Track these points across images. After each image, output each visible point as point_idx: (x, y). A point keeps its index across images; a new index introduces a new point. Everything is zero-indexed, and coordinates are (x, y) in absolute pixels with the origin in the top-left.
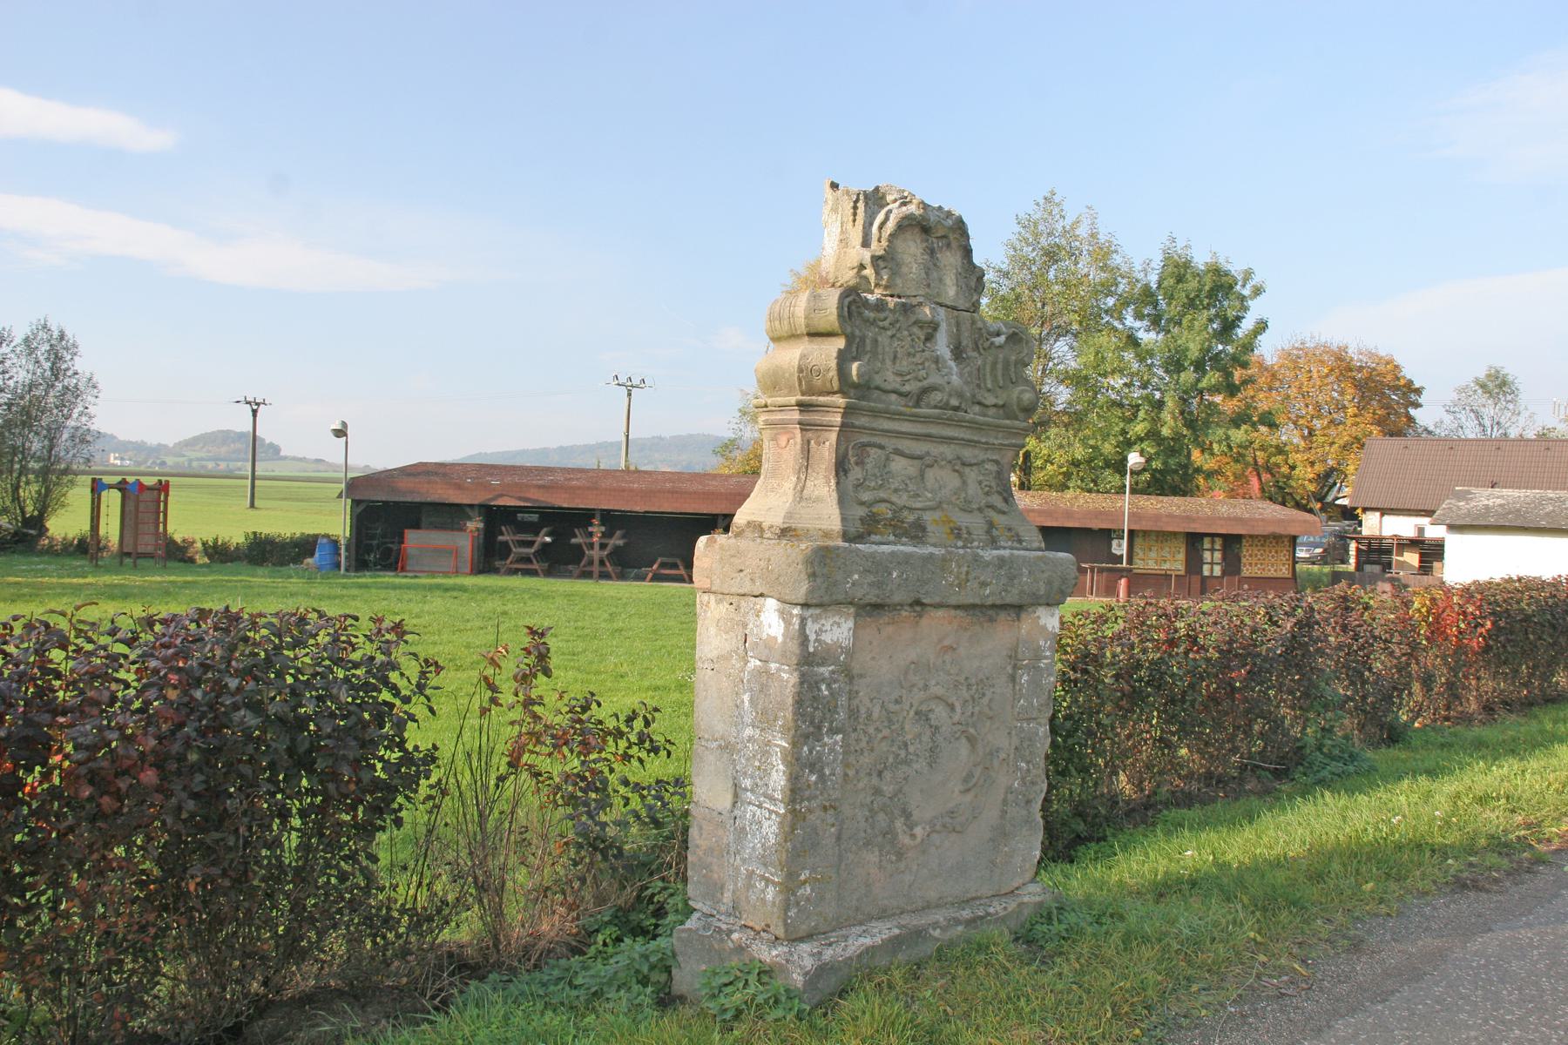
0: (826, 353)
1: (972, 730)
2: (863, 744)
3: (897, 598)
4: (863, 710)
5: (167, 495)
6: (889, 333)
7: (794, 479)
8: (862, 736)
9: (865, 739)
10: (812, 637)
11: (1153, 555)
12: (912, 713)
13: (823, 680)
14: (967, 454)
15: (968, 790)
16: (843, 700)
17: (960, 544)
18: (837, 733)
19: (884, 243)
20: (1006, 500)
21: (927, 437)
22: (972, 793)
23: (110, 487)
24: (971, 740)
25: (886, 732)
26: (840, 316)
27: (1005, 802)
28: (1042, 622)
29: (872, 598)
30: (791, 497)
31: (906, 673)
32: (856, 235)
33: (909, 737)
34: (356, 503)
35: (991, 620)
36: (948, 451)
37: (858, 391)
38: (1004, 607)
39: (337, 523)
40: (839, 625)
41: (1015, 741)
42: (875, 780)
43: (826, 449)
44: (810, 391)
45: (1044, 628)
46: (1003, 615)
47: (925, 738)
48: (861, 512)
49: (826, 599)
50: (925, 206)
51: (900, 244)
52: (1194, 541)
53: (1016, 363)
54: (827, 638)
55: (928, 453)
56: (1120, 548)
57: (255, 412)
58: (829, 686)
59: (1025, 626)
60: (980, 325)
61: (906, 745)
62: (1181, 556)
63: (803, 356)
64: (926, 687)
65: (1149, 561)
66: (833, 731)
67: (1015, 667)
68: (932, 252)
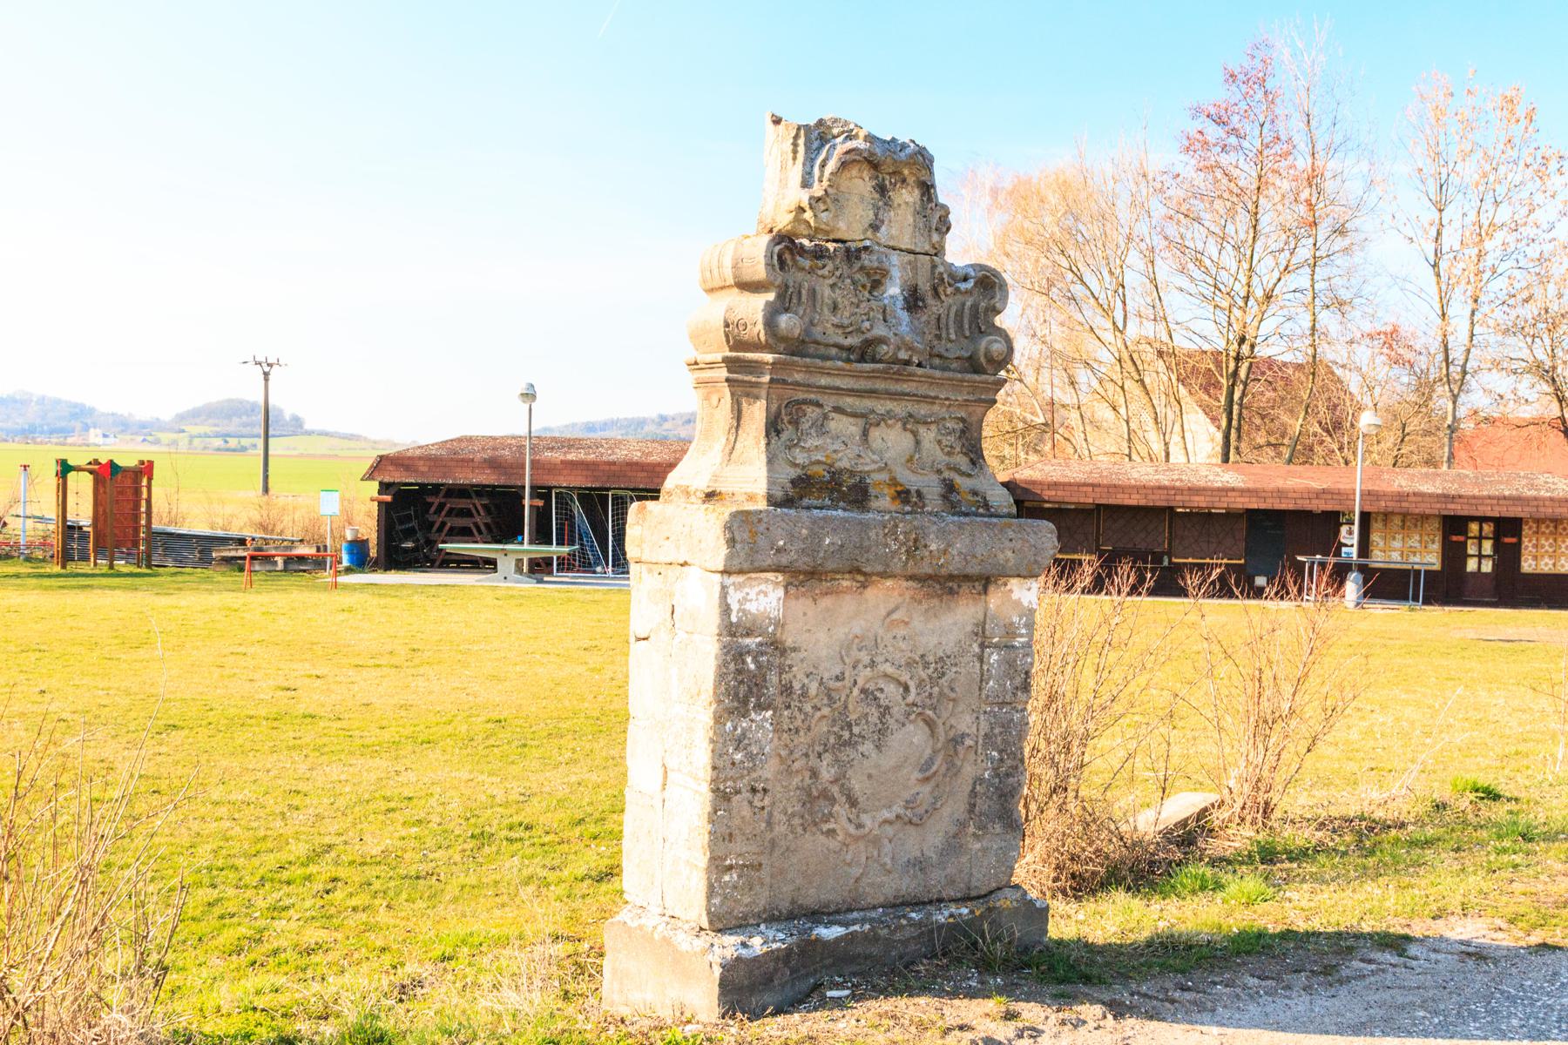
0: (753, 308)
1: (930, 713)
2: (798, 723)
3: (830, 565)
4: (797, 686)
5: (150, 479)
6: (831, 282)
7: (724, 441)
8: (797, 713)
9: (800, 717)
10: (735, 607)
11: (1397, 544)
12: (856, 691)
13: (748, 652)
14: (923, 410)
15: (927, 779)
16: (773, 678)
17: (908, 508)
18: (767, 709)
19: (825, 183)
20: (973, 463)
21: (872, 393)
22: (932, 783)
23: (78, 469)
24: (930, 724)
25: (826, 711)
26: (769, 265)
27: (973, 794)
28: (1015, 596)
29: (804, 562)
30: (728, 465)
31: (849, 648)
32: (796, 172)
33: (853, 717)
34: (385, 487)
35: (951, 592)
36: (899, 408)
37: (796, 347)
38: (967, 578)
39: (355, 509)
40: (766, 594)
41: (984, 727)
42: (814, 761)
43: (757, 413)
44: (739, 345)
45: (1018, 603)
46: (965, 588)
47: (874, 719)
48: (794, 473)
49: (746, 566)
50: (870, 138)
51: (844, 183)
52: (1454, 526)
53: (987, 310)
54: (752, 607)
55: (873, 411)
56: (1349, 537)
57: (266, 374)
58: (755, 660)
59: (994, 600)
60: (941, 269)
61: (850, 726)
62: (1436, 546)
63: (730, 309)
64: (873, 664)
65: (1390, 552)
66: (760, 707)
67: (982, 646)
68: (882, 190)
